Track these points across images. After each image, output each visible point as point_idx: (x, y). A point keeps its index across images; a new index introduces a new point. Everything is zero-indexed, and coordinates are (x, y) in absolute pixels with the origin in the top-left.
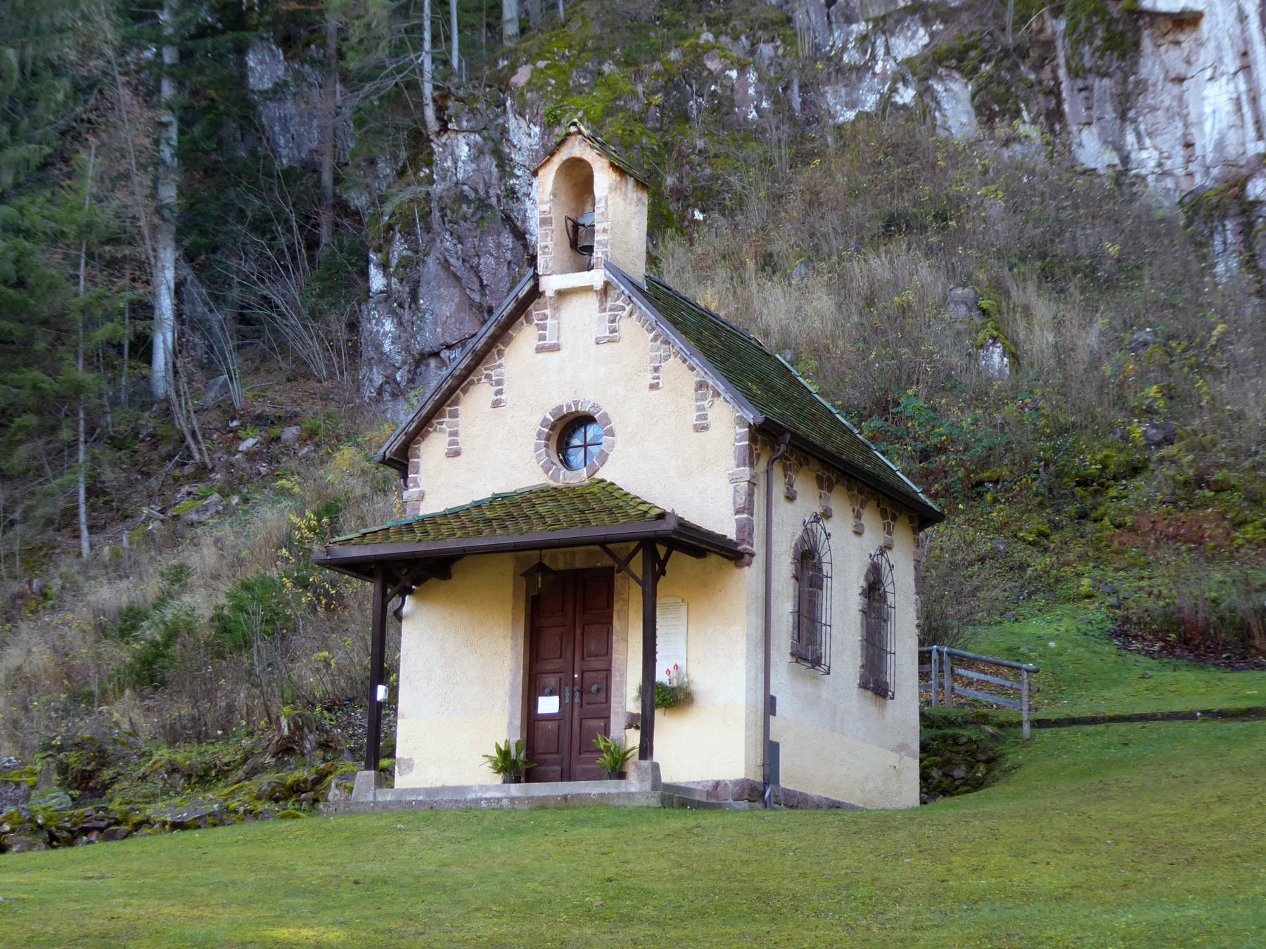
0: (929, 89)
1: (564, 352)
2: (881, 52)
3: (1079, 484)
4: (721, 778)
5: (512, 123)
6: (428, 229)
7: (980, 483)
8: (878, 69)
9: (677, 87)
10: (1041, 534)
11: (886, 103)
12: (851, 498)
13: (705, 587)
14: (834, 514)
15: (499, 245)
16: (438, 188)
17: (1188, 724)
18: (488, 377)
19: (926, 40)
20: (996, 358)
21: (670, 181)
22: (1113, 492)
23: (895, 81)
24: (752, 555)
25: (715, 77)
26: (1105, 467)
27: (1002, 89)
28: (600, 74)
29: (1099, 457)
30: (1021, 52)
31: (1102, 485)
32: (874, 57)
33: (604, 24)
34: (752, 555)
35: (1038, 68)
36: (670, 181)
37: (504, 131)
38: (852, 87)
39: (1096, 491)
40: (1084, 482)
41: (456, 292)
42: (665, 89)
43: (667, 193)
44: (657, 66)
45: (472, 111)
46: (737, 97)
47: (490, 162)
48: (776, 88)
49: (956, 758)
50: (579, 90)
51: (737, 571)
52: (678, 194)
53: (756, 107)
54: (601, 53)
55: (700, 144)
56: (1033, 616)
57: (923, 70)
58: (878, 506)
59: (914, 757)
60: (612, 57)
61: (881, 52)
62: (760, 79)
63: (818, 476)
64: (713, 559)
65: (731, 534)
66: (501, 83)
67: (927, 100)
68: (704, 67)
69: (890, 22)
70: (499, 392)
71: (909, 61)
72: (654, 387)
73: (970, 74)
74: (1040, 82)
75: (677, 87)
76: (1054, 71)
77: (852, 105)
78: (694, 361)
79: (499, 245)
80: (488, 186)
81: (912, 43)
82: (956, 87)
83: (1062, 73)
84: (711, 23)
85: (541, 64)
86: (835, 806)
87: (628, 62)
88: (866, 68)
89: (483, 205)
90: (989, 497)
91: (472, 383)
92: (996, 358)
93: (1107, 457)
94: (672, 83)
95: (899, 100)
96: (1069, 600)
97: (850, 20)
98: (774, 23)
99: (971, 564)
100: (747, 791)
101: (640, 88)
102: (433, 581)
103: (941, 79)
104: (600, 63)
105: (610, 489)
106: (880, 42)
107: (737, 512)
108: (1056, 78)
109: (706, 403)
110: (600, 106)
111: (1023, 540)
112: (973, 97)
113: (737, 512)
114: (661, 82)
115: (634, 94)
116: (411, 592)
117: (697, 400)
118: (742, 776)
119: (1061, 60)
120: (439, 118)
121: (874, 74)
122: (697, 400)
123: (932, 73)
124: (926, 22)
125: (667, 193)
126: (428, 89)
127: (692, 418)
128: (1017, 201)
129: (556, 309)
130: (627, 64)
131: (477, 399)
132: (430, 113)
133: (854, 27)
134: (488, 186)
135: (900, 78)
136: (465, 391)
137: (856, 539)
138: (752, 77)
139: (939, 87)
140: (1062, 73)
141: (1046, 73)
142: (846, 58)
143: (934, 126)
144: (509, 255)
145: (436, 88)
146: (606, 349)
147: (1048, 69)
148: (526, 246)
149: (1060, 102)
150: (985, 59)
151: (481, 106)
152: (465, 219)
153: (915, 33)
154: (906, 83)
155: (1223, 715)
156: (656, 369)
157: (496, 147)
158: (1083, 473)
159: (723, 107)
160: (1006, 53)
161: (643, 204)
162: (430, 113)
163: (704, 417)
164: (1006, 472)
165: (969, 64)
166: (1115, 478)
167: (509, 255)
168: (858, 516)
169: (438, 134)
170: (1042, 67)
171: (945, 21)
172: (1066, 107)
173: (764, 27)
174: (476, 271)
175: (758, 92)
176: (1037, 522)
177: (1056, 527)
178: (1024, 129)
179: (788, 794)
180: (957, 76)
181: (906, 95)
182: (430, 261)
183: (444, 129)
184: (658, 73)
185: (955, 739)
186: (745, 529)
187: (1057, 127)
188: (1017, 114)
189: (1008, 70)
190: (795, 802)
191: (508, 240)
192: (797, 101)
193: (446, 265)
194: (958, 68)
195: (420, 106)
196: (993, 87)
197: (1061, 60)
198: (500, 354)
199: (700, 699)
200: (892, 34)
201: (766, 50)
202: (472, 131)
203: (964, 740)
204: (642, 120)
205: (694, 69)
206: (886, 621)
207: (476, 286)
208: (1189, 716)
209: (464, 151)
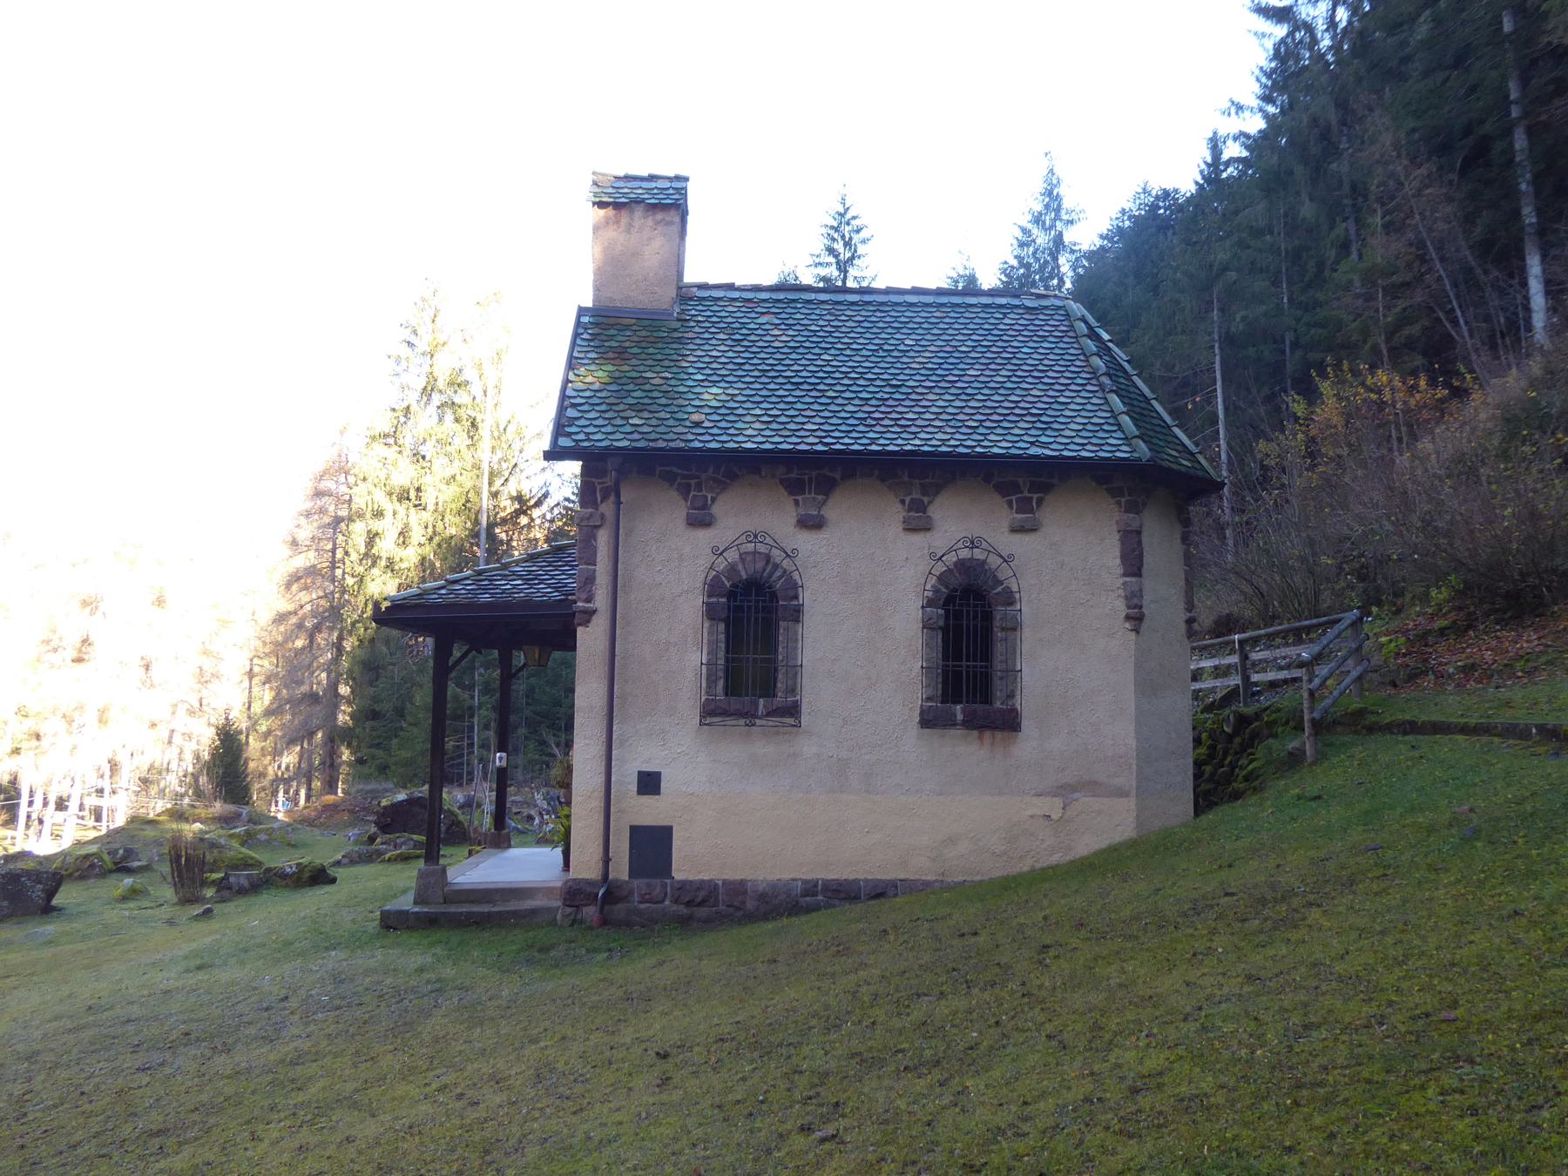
59: (1122, 793)
63: (782, 482)
86: (842, 893)
137: (918, 539)
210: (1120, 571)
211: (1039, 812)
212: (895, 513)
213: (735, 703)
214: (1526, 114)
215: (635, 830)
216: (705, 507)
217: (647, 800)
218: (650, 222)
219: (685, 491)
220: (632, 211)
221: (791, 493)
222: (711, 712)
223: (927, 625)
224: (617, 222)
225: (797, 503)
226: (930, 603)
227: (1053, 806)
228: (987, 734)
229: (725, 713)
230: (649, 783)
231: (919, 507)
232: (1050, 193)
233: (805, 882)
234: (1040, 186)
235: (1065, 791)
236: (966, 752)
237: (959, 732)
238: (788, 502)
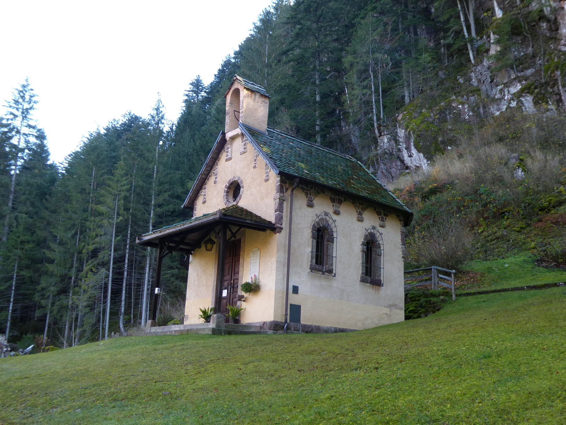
0: (520, 101)
1: (233, 160)
2: (506, 93)
3: (540, 210)
4: (265, 321)
5: (399, 130)
6: (378, 163)
7: (503, 213)
8: (506, 98)
9: (443, 112)
10: (522, 228)
11: (508, 107)
12: (355, 207)
13: (265, 243)
14: (341, 212)
15: (396, 165)
16: (379, 152)
17: (521, 292)
18: (214, 173)
19: (520, 87)
20: (520, 173)
21: (440, 139)
22: (552, 212)
23: (510, 100)
24: (281, 229)
25: (454, 108)
26: (550, 203)
27: (542, 96)
28: (421, 112)
29: (547, 200)
30: (547, 83)
31: (549, 210)
32: (504, 95)
33: (423, 99)
34: (281, 229)
35: (553, 87)
36: (440, 139)
37: (397, 133)
38: (498, 105)
39: (546, 212)
40: (542, 209)
41: (386, 180)
42: (440, 114)
43: (439, 143)
44: (438, 108)
45: (387, 129)
46: (462, 113)
47: (393, 142)
48: (474, 109)
49: (419, 305)
50: (415, 118)
51: (275, 235)
52: (443, 142)
53: (468, 115)
54: (421, 107)
55: (450, 127)
56: (511, 256)
57: (518, 96)
58: (375, 209)
59: (401, 309)
60: (425, 108)
61: (506, 93)
62: (469, 107)
63: (330, 198)
64: (268, 231)
65: (273, 221)
66: (396, 120)
67: (520, 104)
68: (452, 106)
69: (509, 84)
70: (216, 178)
71: (514, 94)
72: (255, 167)
73: (532, 93)
74: (554, 91)
75: (443, 112)
76: (558, 87)
77: (498, 110)
78: (226, 147)
79: (396, 165)
80: (392, 149)
81: (516, 88)
82: (528, 98)
83: (560, 87)
84: (455, 94)
85: (405, 113)
86: (342, 331)
87: (430, 108)
88: (502, 98)
89: (391, 154)
90: (506, 217)
91: (210, 176)
92: (520, 173)
93: (550, 200)
94: (442, 112)
95: (511, 105)
96: (526, 250)
97: (497, 86)
98: (474, 91)
99: (494, 240)
100: (273, 326)
101: (432, 115)
102: (197, 249)
103: (524, 97)
104: (421, 110)
105: (242, 209)
106: (506, 90)
107: (276, 212)
108: (559, 89)
109: (268, 170)
110: (419, 121)
111: (515, 230)
112: (533, 100)
113: (276, 212)
114: (438, 112)
115: (430, 117)
116: (191, 254)
117: (266, 170)
118: (272, 319)
119: (560, 84)
120: (379, 132)
121: (505, 100)
122: (266, 170)
123: (521, 96)
124: (520, 82)
125: (439, 143)
126: (375, 125)
127: (264, 178)
128: (541, 127)
129: (231, 144)
130: (429, 109)
131: (210, 183)
132: (376, 131)
133: (499, 87)
134: (392, 149)
135: (512, 99)
136: (208, 180)
137: (360, 223)
138: (466, 106)
139: (523, 99)
140: (560, 87)
141: (556, 89)
142: (496, 97)
143: (523, 111)
144: (399, 168)
145: (378, 124)
146: (243, 156)
147: (556, 87)
148: (404, 164)
149: (561, 96)
150: (536, 88)
151: (390, 127)
152: (386, 159)
153: (516, 86)
154: (514, 100)
155: (535, 287)
156: (255, 160)
157: (395, 138)
158: (541, 206)
159: (458, 116)
160: (542, 85)
161: (266, 103)
162: (376, 131)
163: (268, 176)
164: (512, 208)
165: (531, 91)
166: (554, 207)
167: (399, 168)
168: (360, 214)
169: (379, 137)
170: (554, 87)
171: (525, 80)
172: (563, 98)
173: (471, 92)
174: (390, 173)
175: (469, 111)
176: (521, 224)
177: (529, 225)
178: (549, 107)
179: (305, 326)
180: (528, 95)
181: (514, 104)
182: (379, 172)
183: (381, 135)
184: (437, 109)
185: (430, 301)
186: (279, 218)
187: (560, 104)
188: (547, 102)
189: (544, 90)
190: (309, 330)
191: (399, 163)
192: (482, 111)
193: (382, 172)
194: (528, 93)
195: (374, 130)
196: (539, 96)
197: (560, 84)
198: (217, 165)
199: (263, 289)
200: (509, 87)
201: (472, 99)
202: (388, 134)
203: (432, 302)
204: (433, 123)
205: (449, 106)
206: (380, 256)
207: (391, 177)
208: (522, 289)
209: (386, 140)
210: (401, 243)
211: (385, 312)
212: (355, 216)
213: (317, 266)
214: (322, 130)
215: (291, 305)
216: (312, 201)
217: (295, 295)
218: (260, 100)
219: (307, 194)
220: (255, 95)
221: (332, 202)
222: (312, 269)
223: (363, 251)
224: (251, 97)
225: (333, 206)
226: (363, 244)
227: (387, 310)
228: (374, 286)
229: (315, 269)
230: (296, 290)
231: (360, 214)
232: (157, 109)
233: (334, 328)
234: (11, 95)
235: (390, 306)
236: (369, 290)
237: (368, 284)
238: (331, 204)
